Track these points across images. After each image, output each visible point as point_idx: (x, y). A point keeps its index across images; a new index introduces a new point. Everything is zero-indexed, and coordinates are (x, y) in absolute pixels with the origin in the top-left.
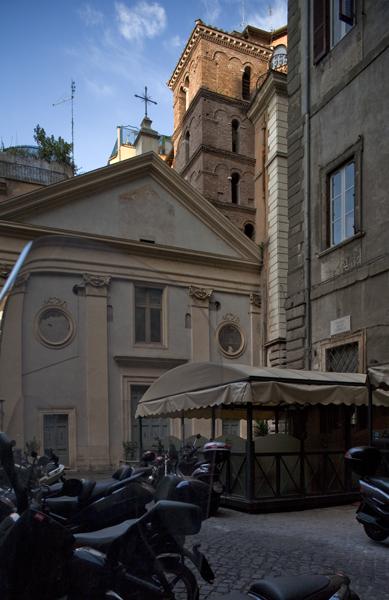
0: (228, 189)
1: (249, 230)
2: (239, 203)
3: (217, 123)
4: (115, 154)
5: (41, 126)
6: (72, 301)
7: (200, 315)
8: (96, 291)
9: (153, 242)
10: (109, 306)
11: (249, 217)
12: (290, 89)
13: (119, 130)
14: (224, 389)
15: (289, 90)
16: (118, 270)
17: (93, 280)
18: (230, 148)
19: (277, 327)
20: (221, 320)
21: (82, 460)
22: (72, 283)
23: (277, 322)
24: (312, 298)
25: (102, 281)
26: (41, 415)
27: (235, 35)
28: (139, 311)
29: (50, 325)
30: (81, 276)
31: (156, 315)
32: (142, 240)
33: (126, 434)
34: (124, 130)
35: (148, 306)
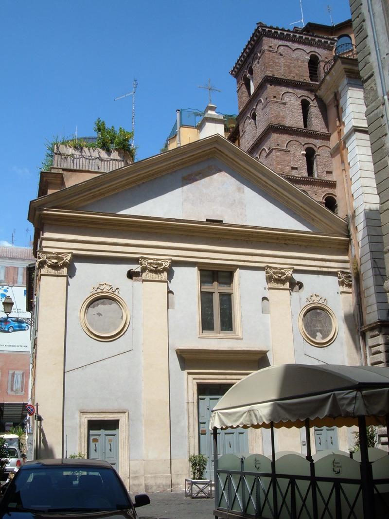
0: (303, 163)
1: (331, 203)
2: (316, 176)
3: (285, 104)
4: (174, 136)
5: (102, 120)
6: (125, 288)
7: (281, 297)
8: (154, 276)
9: (221, 221)
10: (170, 292)
11: (328, 190)
12: (364, 74)
13: (178, 114)
14: (329, 397)
15: (362, 74)
16: (91, 415)
17: (150, 264)
18: (301, 124)
19: (375, 307)
20: (304, 303)
21: (136, 478)
22: (127, 268)
23: (375, 301)
24: (66, 371)
25: (161, 265)
26: (85, 420)
27: (296, 31)
28: (206, 299)
29: (99, 314)
30: (135, 261)
31: (227, 300)
32: (208, 220)
33: (188, 447)
34: (183, 112)
35: (216, 288)
